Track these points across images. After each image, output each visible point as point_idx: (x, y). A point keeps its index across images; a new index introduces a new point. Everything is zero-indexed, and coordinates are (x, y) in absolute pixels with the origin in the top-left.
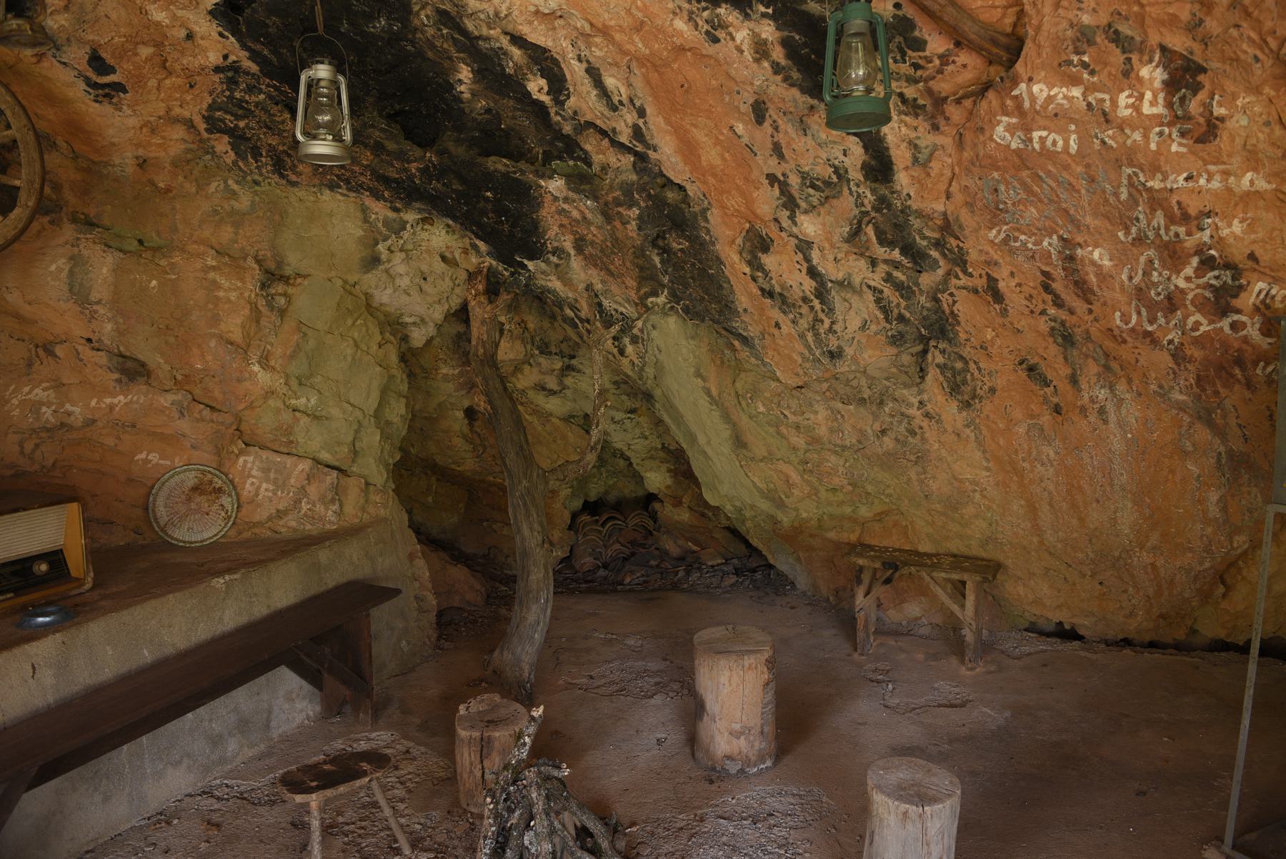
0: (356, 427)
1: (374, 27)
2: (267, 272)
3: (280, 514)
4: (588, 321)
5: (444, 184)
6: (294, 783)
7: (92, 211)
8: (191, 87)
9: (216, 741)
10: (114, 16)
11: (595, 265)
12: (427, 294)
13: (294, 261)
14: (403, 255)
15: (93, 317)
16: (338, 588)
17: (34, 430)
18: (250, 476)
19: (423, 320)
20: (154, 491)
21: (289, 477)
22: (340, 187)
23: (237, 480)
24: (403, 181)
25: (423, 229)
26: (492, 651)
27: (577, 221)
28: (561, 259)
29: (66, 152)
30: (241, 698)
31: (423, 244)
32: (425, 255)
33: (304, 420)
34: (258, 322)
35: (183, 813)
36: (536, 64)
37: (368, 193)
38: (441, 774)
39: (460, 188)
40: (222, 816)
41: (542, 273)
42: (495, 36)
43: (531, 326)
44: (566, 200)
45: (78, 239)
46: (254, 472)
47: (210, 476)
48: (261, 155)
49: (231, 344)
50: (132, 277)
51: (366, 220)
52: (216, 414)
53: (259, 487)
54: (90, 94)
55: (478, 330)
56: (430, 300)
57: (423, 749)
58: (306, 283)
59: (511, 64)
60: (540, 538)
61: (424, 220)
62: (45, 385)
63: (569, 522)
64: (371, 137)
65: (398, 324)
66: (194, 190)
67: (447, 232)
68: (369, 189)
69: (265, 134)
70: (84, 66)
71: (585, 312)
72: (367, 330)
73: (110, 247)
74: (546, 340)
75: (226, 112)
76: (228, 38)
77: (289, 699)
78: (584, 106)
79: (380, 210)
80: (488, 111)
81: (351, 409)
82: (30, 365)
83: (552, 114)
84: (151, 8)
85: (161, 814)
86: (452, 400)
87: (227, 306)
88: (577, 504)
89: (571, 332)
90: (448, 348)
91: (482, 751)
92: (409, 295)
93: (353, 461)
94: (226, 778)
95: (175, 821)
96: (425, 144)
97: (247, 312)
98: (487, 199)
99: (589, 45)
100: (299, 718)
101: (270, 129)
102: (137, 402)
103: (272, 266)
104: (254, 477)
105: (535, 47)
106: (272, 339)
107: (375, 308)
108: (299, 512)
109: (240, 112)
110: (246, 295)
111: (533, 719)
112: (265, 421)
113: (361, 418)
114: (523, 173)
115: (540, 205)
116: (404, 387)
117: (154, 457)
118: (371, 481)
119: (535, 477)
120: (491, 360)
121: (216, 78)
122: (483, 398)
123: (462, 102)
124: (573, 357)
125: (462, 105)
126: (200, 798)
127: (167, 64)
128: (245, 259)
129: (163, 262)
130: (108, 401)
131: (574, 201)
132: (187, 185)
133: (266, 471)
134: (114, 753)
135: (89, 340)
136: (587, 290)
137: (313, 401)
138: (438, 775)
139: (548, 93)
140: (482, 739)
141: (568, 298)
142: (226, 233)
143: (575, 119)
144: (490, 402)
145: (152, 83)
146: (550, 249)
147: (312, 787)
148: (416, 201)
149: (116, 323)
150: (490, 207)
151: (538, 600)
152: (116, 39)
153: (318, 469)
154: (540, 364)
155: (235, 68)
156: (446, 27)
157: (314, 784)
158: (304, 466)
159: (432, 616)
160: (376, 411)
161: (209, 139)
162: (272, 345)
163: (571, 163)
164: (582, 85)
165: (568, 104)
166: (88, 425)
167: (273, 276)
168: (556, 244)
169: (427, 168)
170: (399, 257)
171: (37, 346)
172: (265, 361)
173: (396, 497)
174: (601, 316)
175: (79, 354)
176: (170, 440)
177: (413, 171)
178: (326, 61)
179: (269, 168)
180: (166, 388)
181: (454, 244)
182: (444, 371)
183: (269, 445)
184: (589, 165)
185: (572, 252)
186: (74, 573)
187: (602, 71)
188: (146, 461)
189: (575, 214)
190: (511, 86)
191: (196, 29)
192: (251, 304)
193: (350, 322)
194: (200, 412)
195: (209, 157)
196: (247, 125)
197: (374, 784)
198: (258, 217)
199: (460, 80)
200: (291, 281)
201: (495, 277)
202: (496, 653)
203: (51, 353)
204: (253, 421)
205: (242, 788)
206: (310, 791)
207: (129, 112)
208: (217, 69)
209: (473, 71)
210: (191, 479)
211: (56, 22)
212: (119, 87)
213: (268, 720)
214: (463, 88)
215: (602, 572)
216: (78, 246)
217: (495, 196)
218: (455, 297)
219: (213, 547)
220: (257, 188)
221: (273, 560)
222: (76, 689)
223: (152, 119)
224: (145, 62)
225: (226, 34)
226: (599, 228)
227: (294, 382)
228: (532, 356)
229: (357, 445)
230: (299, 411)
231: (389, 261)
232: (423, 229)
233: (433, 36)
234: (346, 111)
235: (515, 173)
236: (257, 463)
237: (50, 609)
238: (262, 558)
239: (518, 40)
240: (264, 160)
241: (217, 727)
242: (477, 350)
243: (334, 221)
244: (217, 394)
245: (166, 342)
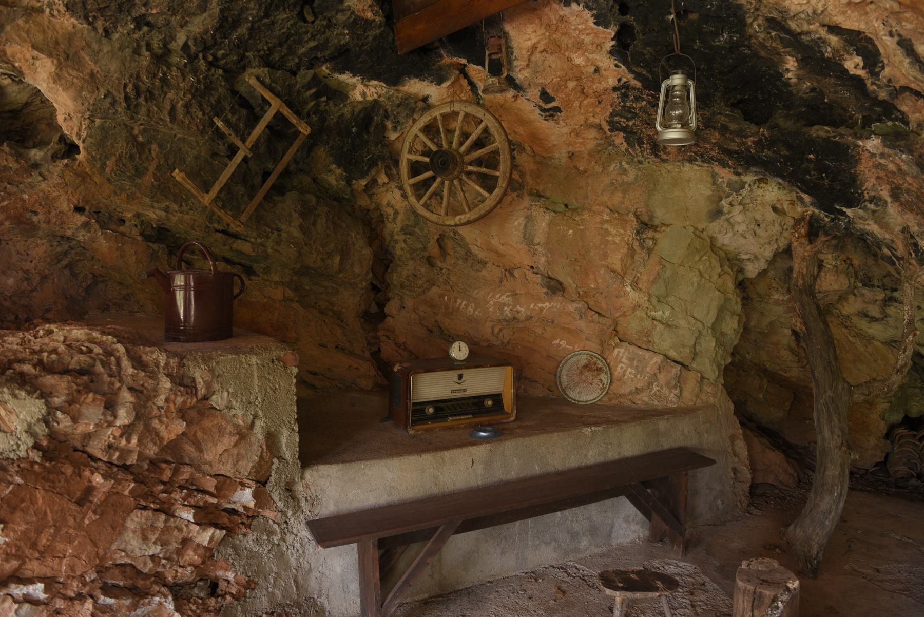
0: (697, 335)
1: (719, 41)
2: (642, 223)
3: (638, 391)
4: (903, 259)
5: (774, 151)
6: (608, 580)
7: (540, 188)
8: (599, 103)
9: (574, 536)
10: (553, 66)
11: (912, 211)
12: (760, 237)
13: (660, 215)
14: (741, 208)
16: (670, 450)
17: (499, 320)
19: (756, 257)
20: (561, 365)
21: (646, 366)
22: (696, 160)
23: (612, 364)
24: (743, 152)
25: (758, 187)
26: (788, 525)
27: (893, 173)
28: (878, 206)
29: (529, 153)
30: (593, 510)
31: (758, 198)
32: (759, 207)
33: (660, 327)
34: (633, 257)
35: (546, 577)
36: (852, 45)
37: (717, 163)
38: (725, 610)
39: (787, 153)
40: (568, 587)
41: (860, 218)
42: (814, 29)
43: (856, 262)
44: (882, 155)
45: (531, 205)
46: (624, 360)
47: (595, 359)
48: (643, 143)
49: (614, 272)
51: (714, 183)
52: (602, 318)
53: (625, 371)
54: (542, 115)
55: (799, 265)
56: (761, 241)
57: (715, 586)
58: (668, 230)
59: (829, 49)
60: (839, 441)
61: (760, 180)
62: (508, 294)
63: (885, 432)
64: (719, 122)
65: (737, 260)
66: (600, 170)
67: (779, 189)
68: (718, 160)
69: (645, 128)
70: (537, 99)
71: (901, 250)
72: (710, 264)
73: (548, 209)
74: (870, 275)
75: (621, 117)
76: (621, 67)
77: (627, 520)
78: (898, 74)
79: (725, 175)
80: (813, 90)
81: (694, 321)
82: (501, 282)
83: (868, 85)
84: (574, 56)
85: (533, 573)
86: (782, 320)
87: (613, 246)
88: (897, 417)
89: (890, 268)
90: (780, 279)
91: (753, 602)
92: (745, 238)
93: (693, 359)
94: (577, 563)
95: (540, 581)
96: (759, 122)
97: (625, 250)
98: (810, 161)
99: (899, 22)
100: (632, 536)
101: (648, 124)
102: (556, 307)
103: (645, 218)
104: (623, 363)
105: (850, 32)
106: (641, 269)
107: (718, 248)
109: (630, 116)
110: (626, 239)
111: (788, 589)
112: (633, 325)
113: (701, 328)
114: (842, 136)
115: (857, 162)
116: (738, 308)
117: (563, 343)
118: (705, 376)
120: (809, 291)
121: (615, 95)
122: (799, 320)
123: (790, 86)
124: (896, 290)
125: (790, 89)
126: (558, 570)
127: (585, 91)
128: (628, 214)
129: (578, 218)
130: (540, 305)
131: (890, 156)
132: (597, 167)
133: (631, 360)
134: (510, 525)
135: (532, 267)
136: (903, 232)
137: (667, 314)
138: (721, 610)
139: (864, 68)
140: (755, 593)
141: (885, 239)
142: (618, 197)
143: (890, 86)
144: (805, 324)
145: (576, 104)
146: (867, 198)
147: (618, 587)
148: (753, 166)
149: (547, 257)
150: (812, 166)
151: (831, 493)
152: (555, 80)
153: (667, 362)
154: (863, 295)
155: (626, 86)
156: (774, 29)
157: (621, 585)
158: (658, 359)
159: (746, 487)
160: (713, 324)
161: (611, 136)
162: (641, 273)
163: (890, 123)
164: (895, 55)
165: (882, 74)
167: (646, 225)
168: (872, 194)
169: (761, 140)
170: (737, 209)
171: (506, 270)
172: (635, 285)
173: (724, 391)
174: (916, 255)
176: (573, 333)
177: (750, 143)
178: (680, 72)
179: (648, 151)
180: (573, 299)
181: (784, 197)
182: (776, 297)
183: (635, 342)
184: (907, 123)
185: (889, 200)
186: (506, 409)
187: (913, 41)
188: (559, 345)
189: (891, 167)
190: (834, 68)
191: (601, 64)
192: (628, 245)
193: (697, 258)
194: (592, 316)
195: (611, 148)
196: (634, 124)
197: (663, 598)
198: (639, 186)
199: (787, 70)
200: (658, 229)
201: (818, 222)
202: (791, 528)
203: (512, 275)
205: (585, 573)
206: (616, 588)
207: (563, 124)
208: (615, 89)
209: (797, 61)
210: (583, 359)
211: (523, 75)
212: (557, 109)
213: (610, 532)
214: (790, 75)
215: (914, 482)
216: (531, 209)
217: (816, 157)
218: (783, 239)
219: (593, 406)
220: (640, 166)
221: (626, 422)
222: (495, 480)
223: (577, 127)
224: (572, 91)
225: (620, 64)
226: (913, 177)
227: (654, 300)
228: (855, 287)
229: (697, 348)
230: (657, 320)
231: (729, 212)
232: (758, 187)
233: (764, 39)
234: (693, 105)
235: (835, 137)
237: (488, 428)
238: (619, 419)
239: (834, 29)
240: (645, 146)
241: (576, 527)
242: (797, 282)
243: (691, 185)
244: (603, 305)
245: (575, 270)
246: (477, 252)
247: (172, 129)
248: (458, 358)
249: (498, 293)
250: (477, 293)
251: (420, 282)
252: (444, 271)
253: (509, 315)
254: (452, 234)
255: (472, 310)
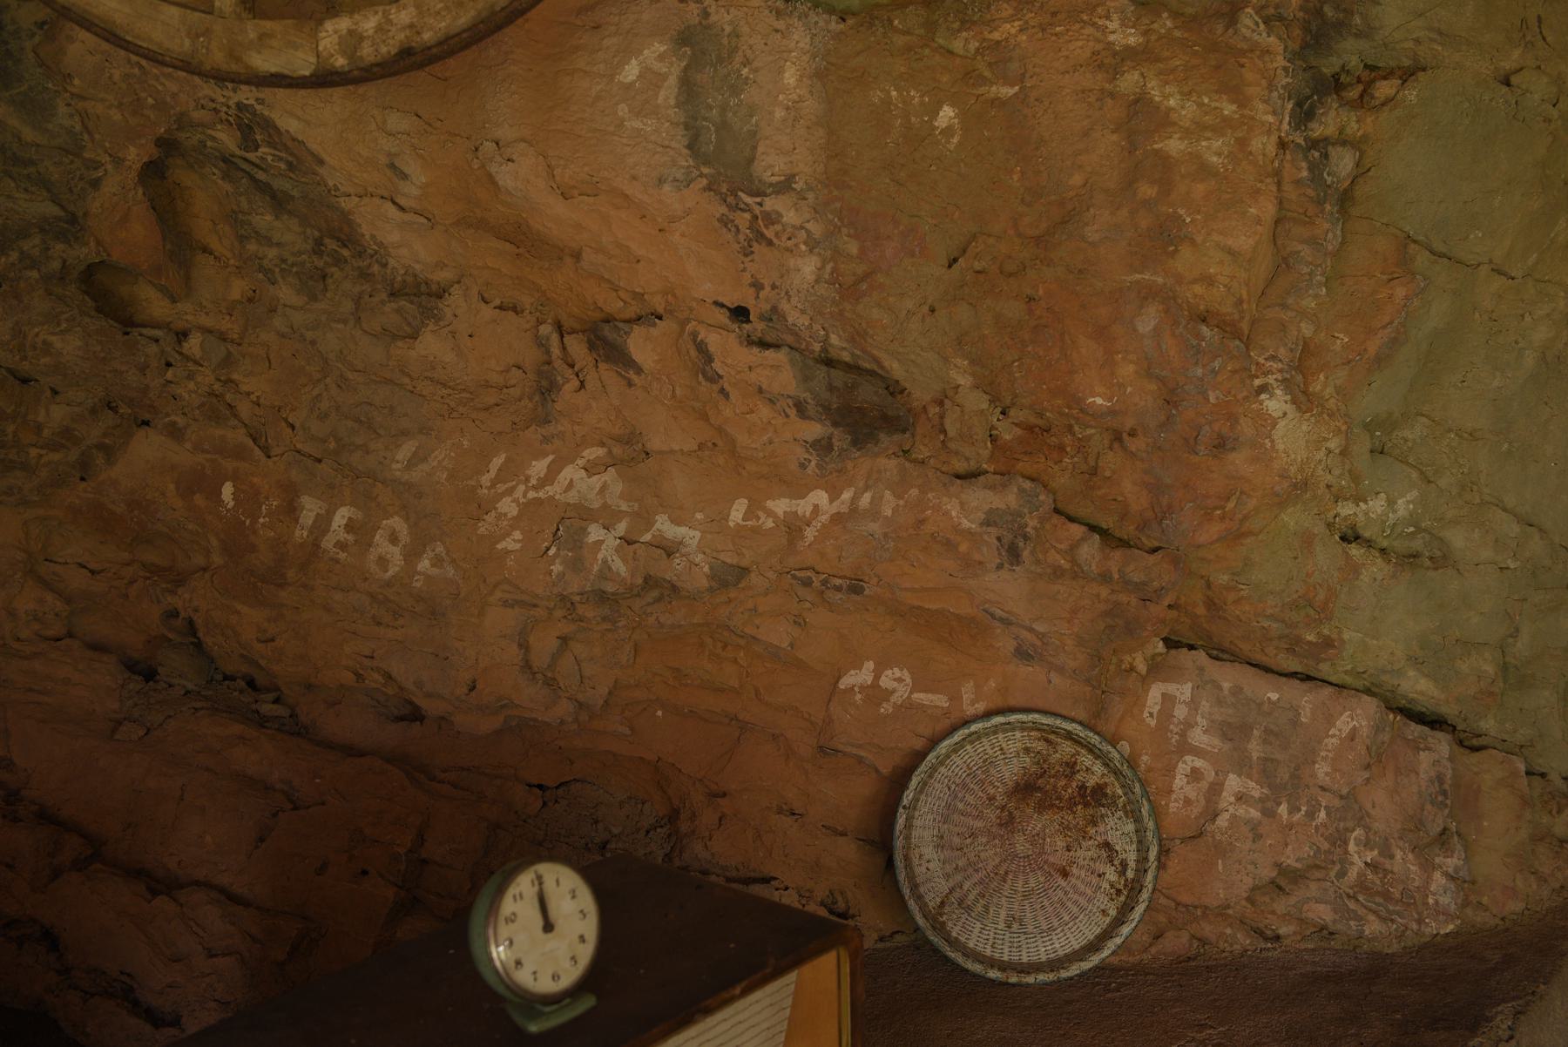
3: (1285, 880)
15: (760, 237)
18: (1185, 748)
33: (1375, 569)
46: (1198, 737)
47: (1067, 748)
50: (876, 96)
52: (1118, 554)
53: (1216, 789)
58: (1411, 95)
62: (593, 453)
82: (547, 388)
87: (1200, 189)
102: (874, 513)
104: (1198, 752)
108: (1342, 874)
119: (214, 170)
130: (780, 506)
133: (1233, 732)
135: (740, 313)
166: (724, 584)
171: (559, 328)
175: (709, 359)
188: (875, 694)
194: (1073, 547)
203: (616, 355)
204: (1224, 578)
236: (1205, 706)
246: (392, 237)
247: (730, 601)
248: (546, 986)
249: (542, 455)
250: (416, 459)
251: (56, 415)
252: (193, 344)
253: (619, 566)
254: (227, 139)
255: (395, 554)
